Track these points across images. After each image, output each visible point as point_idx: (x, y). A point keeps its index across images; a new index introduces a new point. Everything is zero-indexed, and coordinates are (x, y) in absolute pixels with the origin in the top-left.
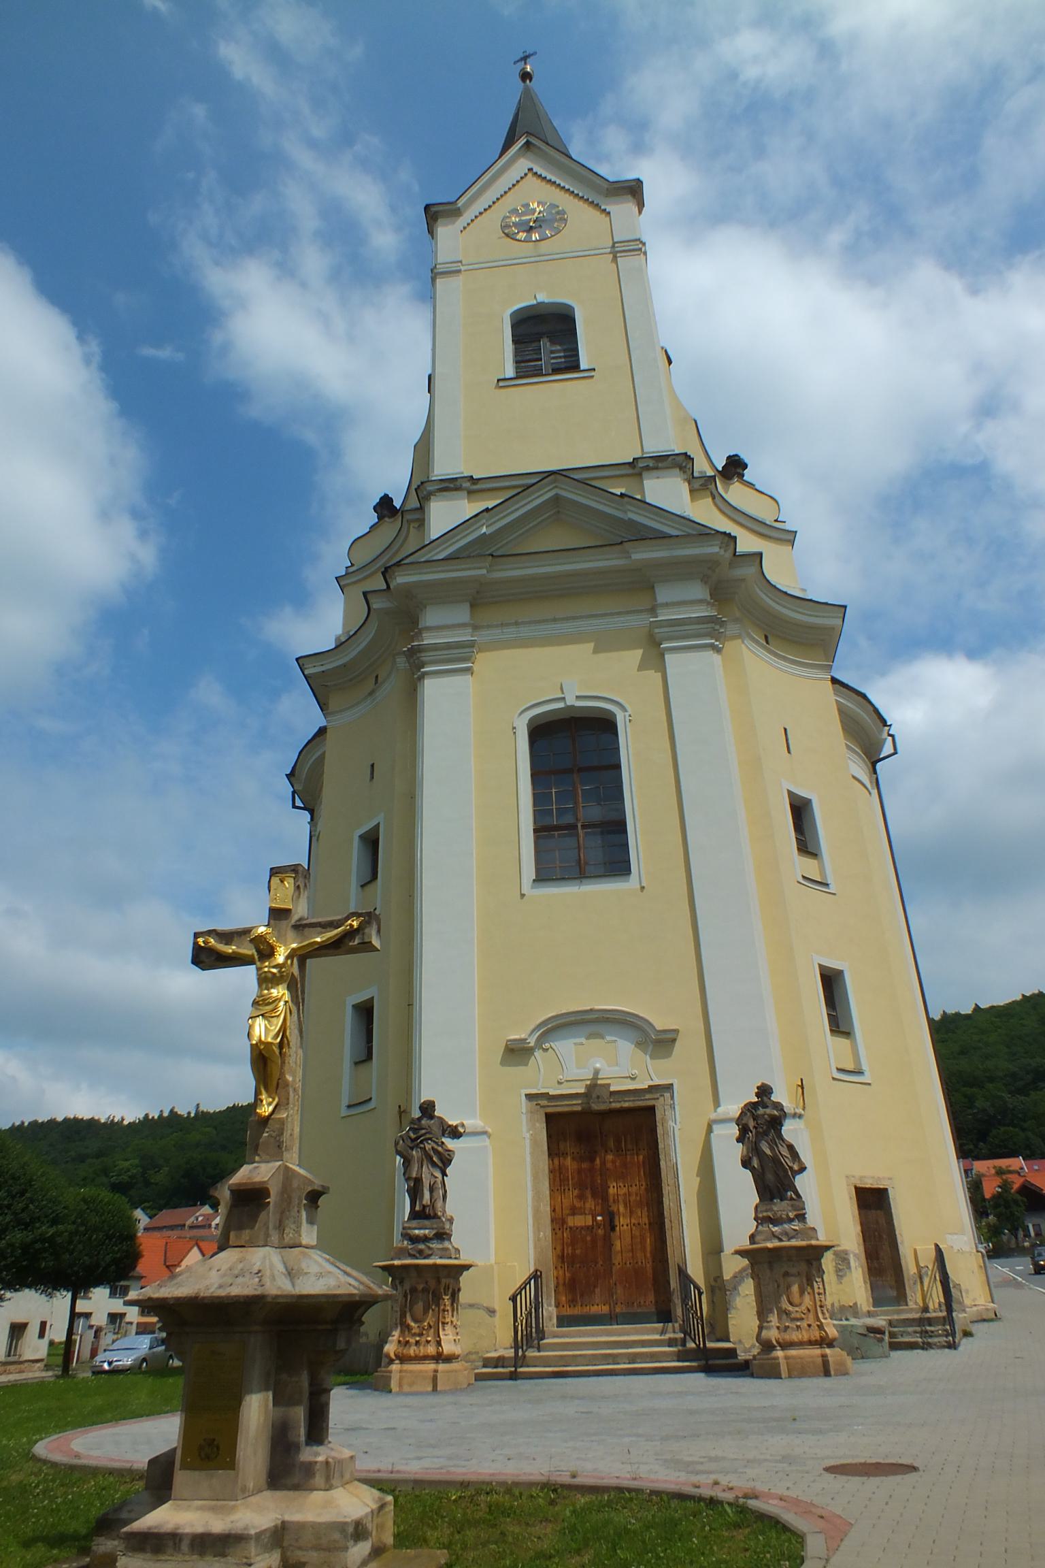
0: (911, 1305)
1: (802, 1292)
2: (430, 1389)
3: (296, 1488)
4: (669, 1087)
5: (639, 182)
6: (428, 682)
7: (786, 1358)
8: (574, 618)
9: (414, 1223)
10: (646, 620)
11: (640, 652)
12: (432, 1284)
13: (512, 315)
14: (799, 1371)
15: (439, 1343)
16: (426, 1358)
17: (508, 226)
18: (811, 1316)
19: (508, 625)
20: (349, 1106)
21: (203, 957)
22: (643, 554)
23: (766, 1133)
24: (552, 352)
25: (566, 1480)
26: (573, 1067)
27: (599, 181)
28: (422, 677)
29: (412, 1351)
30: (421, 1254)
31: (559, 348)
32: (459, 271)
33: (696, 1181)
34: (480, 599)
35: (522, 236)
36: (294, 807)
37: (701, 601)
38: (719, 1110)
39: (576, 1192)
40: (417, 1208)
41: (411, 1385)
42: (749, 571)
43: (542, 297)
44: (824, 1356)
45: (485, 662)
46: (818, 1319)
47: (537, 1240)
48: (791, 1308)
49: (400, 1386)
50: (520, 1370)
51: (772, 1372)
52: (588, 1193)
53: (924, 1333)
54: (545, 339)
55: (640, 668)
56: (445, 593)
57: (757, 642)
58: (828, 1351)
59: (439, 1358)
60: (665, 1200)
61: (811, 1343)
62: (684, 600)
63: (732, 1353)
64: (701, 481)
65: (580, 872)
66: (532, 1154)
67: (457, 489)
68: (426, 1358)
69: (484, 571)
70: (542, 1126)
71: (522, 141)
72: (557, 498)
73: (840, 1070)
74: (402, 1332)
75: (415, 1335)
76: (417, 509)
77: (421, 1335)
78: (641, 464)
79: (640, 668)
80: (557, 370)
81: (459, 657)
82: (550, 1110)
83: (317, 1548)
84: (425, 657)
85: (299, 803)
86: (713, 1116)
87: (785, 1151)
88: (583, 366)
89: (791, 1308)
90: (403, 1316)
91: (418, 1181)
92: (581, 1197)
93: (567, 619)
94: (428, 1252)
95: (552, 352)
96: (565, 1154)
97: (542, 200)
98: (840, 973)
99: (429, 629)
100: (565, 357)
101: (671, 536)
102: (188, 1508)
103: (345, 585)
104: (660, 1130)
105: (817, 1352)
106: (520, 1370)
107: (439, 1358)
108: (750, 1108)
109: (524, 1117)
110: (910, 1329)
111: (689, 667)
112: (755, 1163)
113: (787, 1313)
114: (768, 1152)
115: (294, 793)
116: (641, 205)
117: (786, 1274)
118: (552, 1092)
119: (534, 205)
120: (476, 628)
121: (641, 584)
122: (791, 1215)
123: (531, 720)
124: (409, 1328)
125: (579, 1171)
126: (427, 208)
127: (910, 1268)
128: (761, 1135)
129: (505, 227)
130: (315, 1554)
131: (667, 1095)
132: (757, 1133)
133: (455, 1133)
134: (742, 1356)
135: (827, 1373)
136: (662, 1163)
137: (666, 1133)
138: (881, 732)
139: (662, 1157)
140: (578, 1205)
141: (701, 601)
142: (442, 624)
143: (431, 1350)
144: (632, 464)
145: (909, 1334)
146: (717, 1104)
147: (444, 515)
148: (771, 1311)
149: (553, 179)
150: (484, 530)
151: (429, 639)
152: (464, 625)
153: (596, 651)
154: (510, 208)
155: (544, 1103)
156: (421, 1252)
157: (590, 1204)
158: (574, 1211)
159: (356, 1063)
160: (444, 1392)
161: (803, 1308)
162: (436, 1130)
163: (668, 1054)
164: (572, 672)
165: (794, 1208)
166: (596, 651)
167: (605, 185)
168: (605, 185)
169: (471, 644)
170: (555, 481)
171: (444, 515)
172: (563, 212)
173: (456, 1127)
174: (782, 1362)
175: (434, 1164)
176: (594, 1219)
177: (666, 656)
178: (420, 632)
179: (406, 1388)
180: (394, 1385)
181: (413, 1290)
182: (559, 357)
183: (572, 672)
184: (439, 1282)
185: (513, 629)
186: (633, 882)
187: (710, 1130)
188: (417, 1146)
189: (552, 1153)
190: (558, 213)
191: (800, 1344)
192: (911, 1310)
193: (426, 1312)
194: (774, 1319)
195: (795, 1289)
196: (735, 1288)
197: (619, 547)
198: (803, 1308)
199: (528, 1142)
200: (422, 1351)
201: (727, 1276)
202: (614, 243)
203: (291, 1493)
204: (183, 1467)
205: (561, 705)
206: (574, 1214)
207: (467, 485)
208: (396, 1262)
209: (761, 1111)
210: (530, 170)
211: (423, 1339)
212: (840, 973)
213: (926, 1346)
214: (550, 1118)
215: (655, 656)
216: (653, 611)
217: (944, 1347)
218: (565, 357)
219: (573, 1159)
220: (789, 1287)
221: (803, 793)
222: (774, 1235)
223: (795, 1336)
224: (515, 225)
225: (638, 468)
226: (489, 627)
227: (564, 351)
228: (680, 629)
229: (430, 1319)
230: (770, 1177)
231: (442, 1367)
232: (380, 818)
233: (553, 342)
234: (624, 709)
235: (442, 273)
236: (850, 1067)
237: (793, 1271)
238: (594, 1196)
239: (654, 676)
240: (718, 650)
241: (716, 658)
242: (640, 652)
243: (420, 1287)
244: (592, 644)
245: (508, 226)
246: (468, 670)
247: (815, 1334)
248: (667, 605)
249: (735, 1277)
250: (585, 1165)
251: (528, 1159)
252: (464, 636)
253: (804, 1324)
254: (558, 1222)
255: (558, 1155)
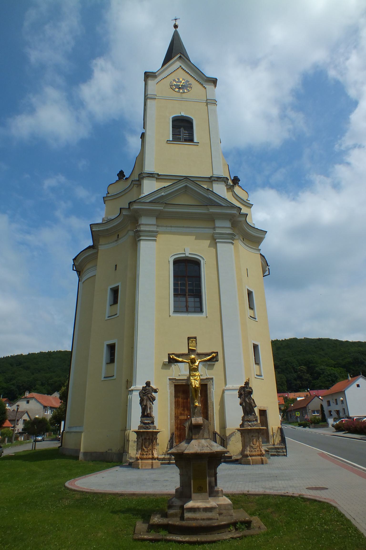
0: (271, 443)
1: (256, 442)
2: (151, 467)
3: (215, 496)
4: (212, 379)
5: (216, 79)
6: (142, 242)
7: (252, 459)
8: (189, 227)
9: (145, 419)
10: (211, 231)
11: (209, 241)
12: (151, 437)
13: (173, 118)
14: (255, 463)
15: (153, 454)
16: (149, 459)
17: (172, 86)
18: (258, 448)
19: (169, 226)
20: (105, 377)
21: (172, 361)
22: (213, 210)
23: (247, 396)
24: (184, 133)
25: (247, 493)
26: (181, 371)
27: (204, 76)
28: (140, 240)
29: (145, 457)
30: (147, 428)
31: (187, 132)
32: (155, 98)
33: (218, 407)
34: (160, 216)
35: (177, 90)
36: (73, 270)
37: (229, 228)
38: (227, 386)
39: (182, 409)
40: (145, 414)
41: (145, 466)
42: (243, 219)
43: (183, 114)
44: (262, 459)
45: (161, 238)
46: (260, 449)
47: (171, 423)
48: (253, 446)
49: (142, 467)
50: (171, 462)
51: (248, 463)
52: (186, 409)
53: (277, 452)
54: (183, 128)
55: (209, 247)
56: (149, 213)
57: (241, 241)
58: (263, 457)
59: (153, 458)
60: (209, 412)
61: (258, 455)
62: (224, 227)
63: (231, 457)
64: (230, 186)
65: (187, 310)
66: (170, 397)
67: (152, 177)
68: (149, 459)
69: (162, 208)
70: (173, 388)
71: (179, 56)
72: (186, 186)
73: (257, 375)
74: (141, 451)
75: (146, 452)
76: (137, 181)
77: (147, 452)
78: (213, 179)
79: (209, 247)
80: (186, 140)
81: (153, 235)
82: (176, 384)
83: (225, 509)
84: (141, 234)
85: (74, 269)
86: (225, 388)
87: (252, 401)
88: (195, 141)
89: (253, 446)
90: (142, 446)
91: (146, 406)
92: (184, 410)
93: (187, 227)
94: (149, 427)
95: (184, 133)
96: (179, 397)
97: (184, 79)
98: (257, 346)
99: (143, 224)
100: (189, 136)
101: (222, 206)
102: (198, 502)
103: (106, 200)
104: (208, 391)
105: (260, 458)
106: (171, 462)
107: (153, 458)
108: (242, 388)
109: (168, 385)
110: (273, 451)
111: (224, 248)
112: (244, 404)
113: (252, 447)
114: (248, 401)
115: (73, 265)
116: (215, 86)
117: (253, 436)
118: (177, 378)
119: (181, 80)
120: (158, 226)
121: (211, 219)
122: (254, 420)
123: (174, 259)
124: (144, 450)
125: (183, 402)
126: (145, 73)
127: (271, 433)
128: (246, 396)
129: (171, 86)
130: (225, 511)
131: (211, 381)
132: (245, 396)
133: (156, 391)
134: (233, 458)
135: (262, 463)
136: (209, 401)
137: (210, 392)
138: (266, 268)
139: (209, 399)
140: (182, 412)
141: (229, 228)
142: (147, 223)
143: (151, 456)
144: (210, 178)
145: (273, 452)
146: (226, 384)
147: (149, 187)
148: (248, 446)
149: (188, 72)
150: (163, 194)
151: (143, 228)
152: (154, 225)
153: (196, 239)
154: (173, 79)
155: (174, 381)
156: (147, 427)
157: (186, 412)
158: (181, 414)
159: (107, 363)
160: (155, 469)
161: (257, 445)
162: (151, 390)
163: (212, 369)
164: (188, 245)
165: (255, 418)
166: (196, 239)
167: (206, 78)
168: (206, 78)
169: (157, 232)
170: (186, 181)
171: (149, 187)
172: (191, 84)
173: (156, 389)
174: (251, 460)
175: (151, 401)
176: (187, 417)
177: (218, 244)
178: (140, 225)
179: (143, 468)
180: (140, 467)
181: (145, 439)
182: (186, 136)
183: (188, 245)
184: (153, 436)
185: (170, 228)
186: (204, 315)
187: (223, 392)
188: (145, 395)
189: (176, 396)
190: (189, 84)
191: (255, 455)
192: (271, 445)
193: (149, 445)
194: (248, 449)
195: (255, 440)
196: (229, 439)
197: (205, 207)
198: (257, 445)
199: (169, 393)
200: (148, 457)
201: (227, 435)
202: (207, 99)
203: (214, 498)
204: (194, 492)
205: (184, 255)
206: (181, 415)
207: (156, 176)
208: (141, 430)
209: (247, 390)
210: (180, 66)
211: (148, 453)
212: (257, 346)
213: (278, 455)
214: (176, 386)
215: (214, 243)
216: (214, 228)
217: (283, 456)
218: (189, 136)
219: (182, 398)
220: (253, 440)
221: (256, 343)
222: (249, 425)
223: (254, 453)
224: (175, 85)
225: (212, 180)
226: (162, 226)
227: (189, 133)
228: (223, 236)
229: (150, 447)
230: (248, 408)
231: (154, 461)
232: (119, 284)
233: (185, 130)
234: (203, 259)
235: (149, 98)
236: (258, 374)
237: (254, 435)
238: (187, 410)
239: (213, 250)
240: (233, 244)
241: (232, 246)
242: (209, 241)
243: (148, 438)
244: (195, 237)
245: (172, 86)
246: (155, 240)
247: (259, 453)
248: (219, 227)
249: (230, 435)
250: (185, 401)
251: (169, 398)
252: (154, 228)
253: (256, 450)
254: (177, 417)
255: (177, 397)
